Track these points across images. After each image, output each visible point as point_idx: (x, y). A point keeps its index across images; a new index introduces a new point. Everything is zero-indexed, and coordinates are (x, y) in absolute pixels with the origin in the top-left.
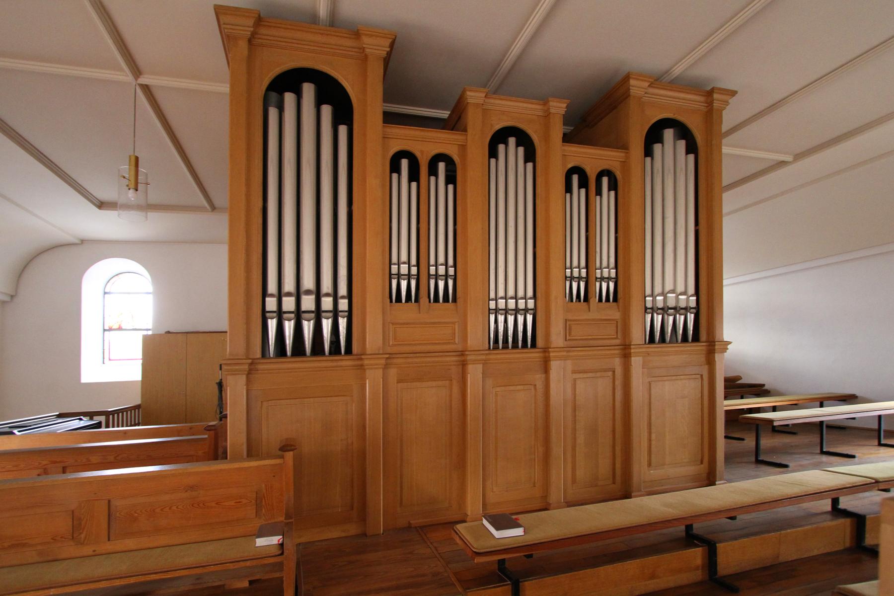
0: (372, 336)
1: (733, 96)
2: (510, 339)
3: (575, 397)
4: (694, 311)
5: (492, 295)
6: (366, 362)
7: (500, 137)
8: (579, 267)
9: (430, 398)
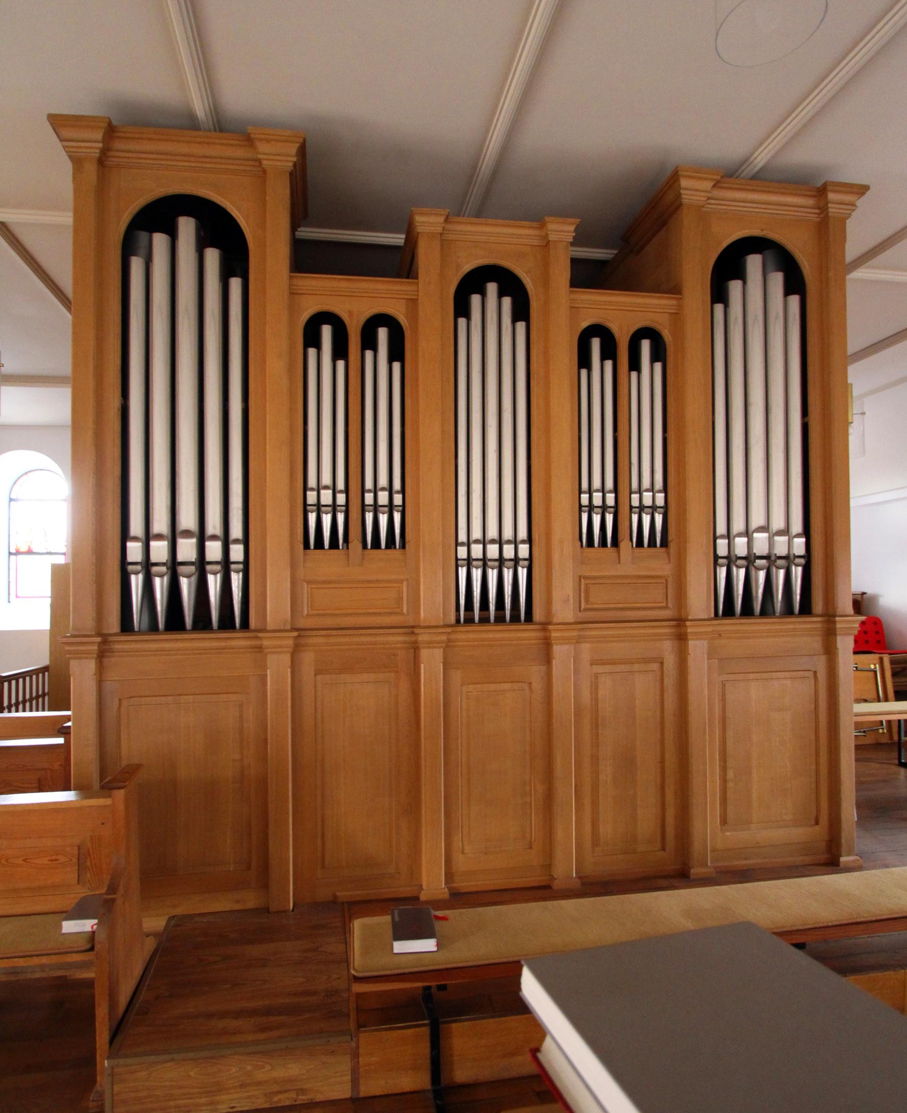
0: (275, 603)
1: (863, 194)
2: (492, 607)
3: (597, 704)
4: (802, 561)
5: (462, 537)
6: (266, 643)
7: (473, 283)
8: (603, 490)
9: (360, 702)
